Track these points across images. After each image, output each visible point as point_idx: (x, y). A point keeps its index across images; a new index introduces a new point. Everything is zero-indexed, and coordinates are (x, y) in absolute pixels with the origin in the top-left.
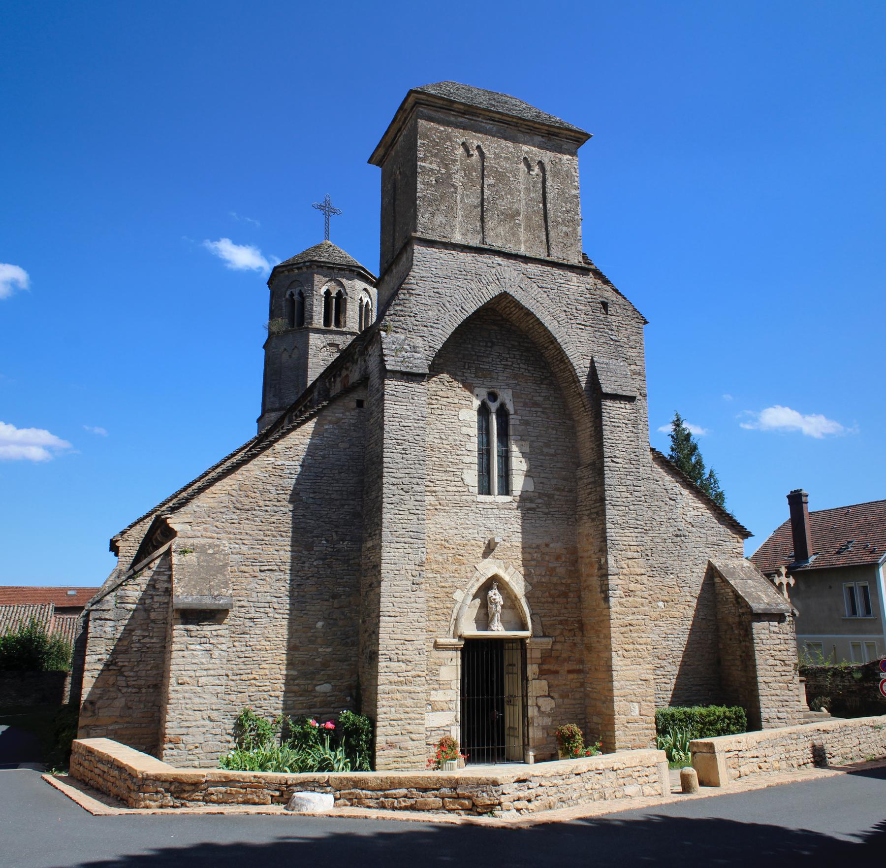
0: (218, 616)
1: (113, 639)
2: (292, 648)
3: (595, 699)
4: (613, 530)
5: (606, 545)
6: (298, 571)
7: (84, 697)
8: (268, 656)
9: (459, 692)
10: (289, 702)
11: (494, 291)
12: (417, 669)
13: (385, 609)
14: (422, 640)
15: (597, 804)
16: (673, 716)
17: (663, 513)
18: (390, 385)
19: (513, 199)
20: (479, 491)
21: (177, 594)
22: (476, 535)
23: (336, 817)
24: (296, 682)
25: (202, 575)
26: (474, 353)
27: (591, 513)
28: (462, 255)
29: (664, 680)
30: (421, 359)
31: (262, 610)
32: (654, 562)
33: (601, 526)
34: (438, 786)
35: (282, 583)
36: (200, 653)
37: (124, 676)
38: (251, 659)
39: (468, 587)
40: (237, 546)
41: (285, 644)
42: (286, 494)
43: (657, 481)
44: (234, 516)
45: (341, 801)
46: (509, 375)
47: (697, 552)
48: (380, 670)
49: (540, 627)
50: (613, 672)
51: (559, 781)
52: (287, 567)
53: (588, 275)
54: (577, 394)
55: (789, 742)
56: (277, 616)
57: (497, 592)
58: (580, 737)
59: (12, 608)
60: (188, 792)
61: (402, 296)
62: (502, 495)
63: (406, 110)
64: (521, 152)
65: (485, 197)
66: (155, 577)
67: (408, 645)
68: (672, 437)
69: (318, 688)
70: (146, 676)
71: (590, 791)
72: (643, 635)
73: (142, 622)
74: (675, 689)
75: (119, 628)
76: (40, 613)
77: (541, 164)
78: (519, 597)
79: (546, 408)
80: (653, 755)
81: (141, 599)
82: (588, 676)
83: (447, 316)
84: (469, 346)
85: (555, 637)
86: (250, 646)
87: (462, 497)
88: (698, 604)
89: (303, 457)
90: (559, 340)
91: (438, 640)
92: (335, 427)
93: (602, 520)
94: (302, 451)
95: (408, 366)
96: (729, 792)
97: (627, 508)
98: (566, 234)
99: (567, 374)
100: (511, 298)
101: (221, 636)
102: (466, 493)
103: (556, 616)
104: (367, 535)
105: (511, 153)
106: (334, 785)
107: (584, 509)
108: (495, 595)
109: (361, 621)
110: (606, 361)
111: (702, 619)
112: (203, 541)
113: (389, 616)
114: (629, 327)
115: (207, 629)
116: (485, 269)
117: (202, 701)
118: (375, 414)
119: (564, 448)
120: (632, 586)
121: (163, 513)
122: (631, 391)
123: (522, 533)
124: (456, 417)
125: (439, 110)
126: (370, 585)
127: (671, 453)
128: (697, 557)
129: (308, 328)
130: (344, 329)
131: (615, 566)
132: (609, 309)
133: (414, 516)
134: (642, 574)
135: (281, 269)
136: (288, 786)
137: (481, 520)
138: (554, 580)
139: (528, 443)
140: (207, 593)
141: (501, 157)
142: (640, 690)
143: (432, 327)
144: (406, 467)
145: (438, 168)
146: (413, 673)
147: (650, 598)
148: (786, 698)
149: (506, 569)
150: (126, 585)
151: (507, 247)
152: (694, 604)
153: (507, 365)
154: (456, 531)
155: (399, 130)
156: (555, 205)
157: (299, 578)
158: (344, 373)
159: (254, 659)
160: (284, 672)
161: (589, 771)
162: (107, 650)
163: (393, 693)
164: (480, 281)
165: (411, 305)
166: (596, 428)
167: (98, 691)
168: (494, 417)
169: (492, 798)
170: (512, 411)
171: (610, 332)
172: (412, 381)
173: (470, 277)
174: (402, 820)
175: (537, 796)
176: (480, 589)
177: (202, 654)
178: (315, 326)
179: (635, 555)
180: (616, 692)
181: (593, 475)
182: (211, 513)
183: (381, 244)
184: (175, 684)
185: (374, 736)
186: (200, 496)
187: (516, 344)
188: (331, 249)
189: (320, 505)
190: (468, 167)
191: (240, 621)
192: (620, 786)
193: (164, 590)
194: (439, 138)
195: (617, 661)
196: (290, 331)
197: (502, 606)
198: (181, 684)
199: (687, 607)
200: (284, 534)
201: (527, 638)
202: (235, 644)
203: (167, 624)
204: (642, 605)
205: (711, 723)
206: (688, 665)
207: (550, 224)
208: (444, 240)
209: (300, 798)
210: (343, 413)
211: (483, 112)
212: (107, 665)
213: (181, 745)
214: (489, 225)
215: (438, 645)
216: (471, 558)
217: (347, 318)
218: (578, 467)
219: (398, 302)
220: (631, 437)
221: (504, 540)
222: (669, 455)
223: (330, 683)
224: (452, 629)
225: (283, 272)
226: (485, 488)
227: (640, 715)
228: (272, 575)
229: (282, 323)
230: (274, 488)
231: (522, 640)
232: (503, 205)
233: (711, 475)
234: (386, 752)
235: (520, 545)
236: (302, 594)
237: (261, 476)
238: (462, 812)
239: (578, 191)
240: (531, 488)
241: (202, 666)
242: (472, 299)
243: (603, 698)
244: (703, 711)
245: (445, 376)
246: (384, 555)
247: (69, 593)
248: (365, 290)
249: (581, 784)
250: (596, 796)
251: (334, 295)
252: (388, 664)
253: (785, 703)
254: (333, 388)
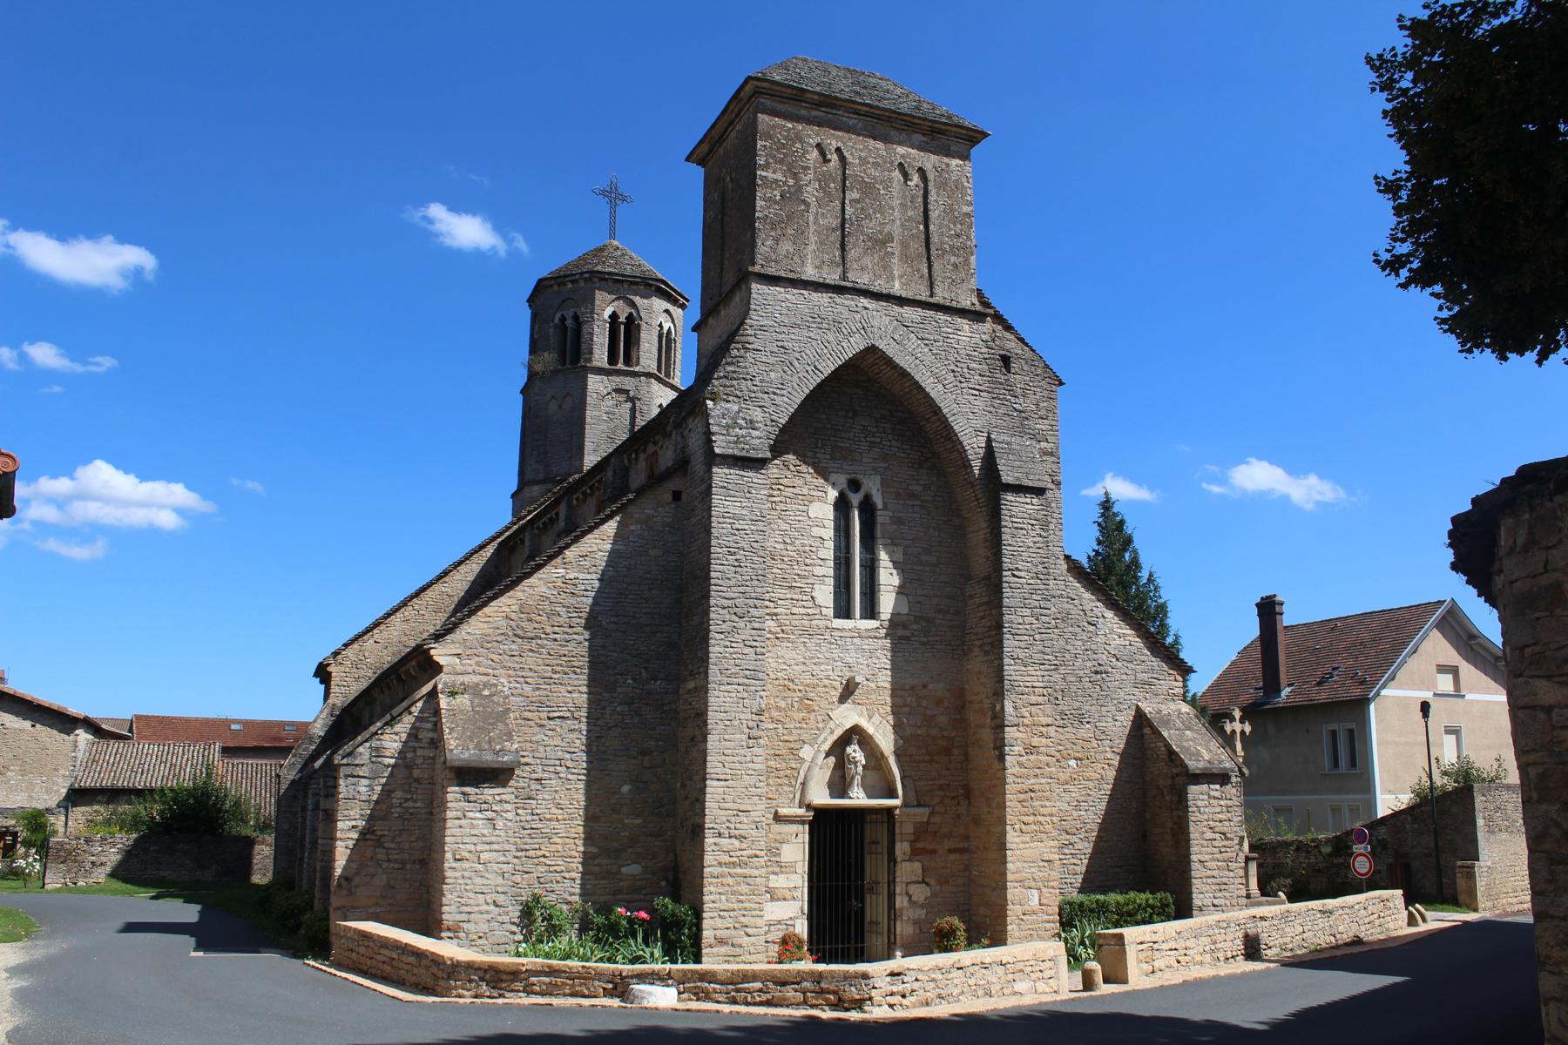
0: (501, 777)
2: (590, 819)
3: (982, 886)
4: (1012, 668)
5: (1003, 687)
6: (597, 719)
7: (338, 872)
8: (560, 827)
9: (806, 877)
10: (588, 887)
11: (857, 344)
12: (754, 847)
13: (712, 771)
14: (760, 811)
15: (981, 1001)
16: (1081, 905)
17: (1080, 643)
18: (720, 474)
19: (884, 219)
20: (834, 613)
21: (450, 747)
22: (831, 673)
23: (683, 1010)
24: (597, 861)
28: (815, 296)
29: (1073, 861)
30: (760, 438)
31: (552, 769)
34: (798, 979)
35: (576, 735)
36: (480, 822)
37: (384, 848)
38: (539, 831)
40: (518, 685)
41: (581, 813)
42: (580, 618)
43: (1073, 599)
44: (513, 647)
45: (685, 996)
47: (1122, 694)
48: (707, 848)
50: (1007, 852)
53: (984, 322)
54: (968, 483)
56: (570, 777)
57: (857, 747)
58: (963, 933)
59: (166, 747)
60: (506, 981)
61: (735, 352)
62: (866, 618)
63: (741, 100)
64: (895, 156)
65: (847, 217)
66: (418, 724)
67: (742, 816)
68: (1099, 524)
69: (624, 870)
71: (974, 987)
72: (1048, 804)
74: (1087, 871)
75: (375, 788)
76: (203, 756)
77: (921, 172)
78: (886, 755)
79: (926, 501)
80: (1050, 947)
82: (975, 856)
83: (795, 378)
84: (824, 416)
86: (537, 814)
87: (812, 622)
88: (1120, 762)
89: (602, 568)
90: (945, 411)
91: (779, 810)
92: (644, 527)
94: (601, 560)
95: (743, 449)
96: (1136, 988)
97: (1031, 638)
98: (955, 266)
99: (955, 455)
102: (817, 617)
104: (688, 673)
108: (855, 751)
109: (678, 785)
111: (1125, 781)
112: (476, 679)
114: (1038, 390)
115: (489, 793)
116: (846, 314)
117: (485, 882)
119: (950, 555)
120: (1035, 741)
121: (426, 642)
123: (892, 670)
124: (804, 514)
126: (692, 739)
128: (1121, 700)
129: (586, 366)
130: (637, 369)
131: (1014, 714)
133: (750, 649)
134: (1049, 725)
135: (547, 283)
136: (623, 978)
137: (836, 653)
138: (934, 732)
139: (900, 549)
140: (486, 747)
141: (868, 163)
142: (1041, 874)
143: (774, 393)
144: (740, 583)
145: (784, 179)
146: (749, 852)
150: (382, 734)
151: (876, 284)
152: (1116, 763)
153: (874, 442)
154: (804, 668)
155: (731, 123)
156: (940, 226)
157: (598, 728)
158: (651, 449)
159: (543, 831)
160: (581, 849)
161: (974, 964)
162: (362, 815)
164: (839, 330)
165: (747, 364)
167: (354, 866)
168: (856, 513)
169: (862, 992)
170: (880, 504)
171: (1013, 400)
173: (826, 326)
175: (913, 991)
177: (483, 824)
178: (595, 364)
179: (1040, 699)
180: (1010, 877)
181: (988, 593)
182: (484, 641)
183: (703, 272)
184: (452, 861)
186: (470, 620)
187: (888, 413)
188: (619, 253)
189: (624, 632)
191: (525, 783)
192: (1009, 982)
193: (429, 740)
194: (786, 138)
195: (1012, 837)
196: (560, 370)
197: (864, 766)
198: (459, 860)
199: (1106, 766)
200: (578, 670)
201: (896, 807)
202: (518, 811)
204: (1048, 765)
205: (1129, 914)
206: (1106, 841)
207: (933, 252)
208: (791, 275)
209: (640, 990)
210: (654, 509)
211: (845, 104)
213: (462, 935)
214: (852, 254)
215: (780, 816)
217: (641, 353)
218: (969, 580)
219: (729, 360)
221: (867, 680)
222: (1094, 550)
223: (640, 864)
224: (798, 796)
225: (551, 286)
226: (843, 610)
227: (1040, 905)
228: (563, 725)
229: (548, 358)
230: (564, 609)
231: (889, 811)
232: (870, 227)
233: (1150, 580)
234: (715, 950)
235: (888, 686)
236: (602, 749)
237: (548, 593)
238: (826, 1008)
240: (905, 610)
241: (484, 839)
242: (828, 355)
244: (1120, 898)
245: (790, 457)
246: (713, 701)
247: (233, 727)
248: (667, 311)
249: (964, 979)
250: (980, 992)
251: (622, 319)
252: (717, 840)
253: (1223, 887)
254: (633, 466)
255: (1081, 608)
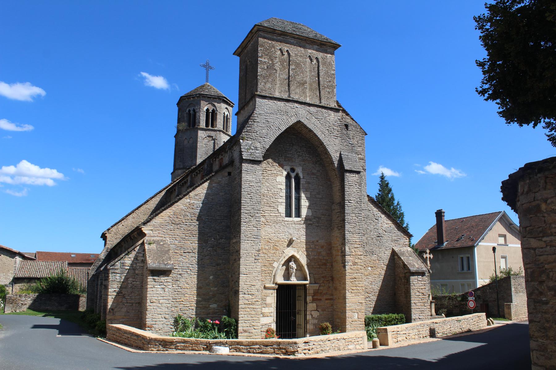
0: (167, 273)
1: (120, 282)
2: (199, 288)
3: (338, 312)
6: (201, 253)
7: (109, 307)
9: (275, 308)
10: (198, 312)
11: (293, 120)
12: (257, 298)
13: (242, 271)
14: (259, 285)
16: (373, 318)
17: (372, 226)
18: (245, 166)
23: (231, 355)
24: (201, 303)
25: (159, 254)
26: (284, 149)
27: (338, 226)
28: (279, 103)
29: (369, 303)
30: (259, 153)
31: (185, 270)
32: (367, 249)
33: (343, 233)
36: (160, 289)
37: (126, 298)
39: (280, 261)
40: (173, 241)
42: (195, 217)
43: (370, 211)
44: (171, 227)
45: (232, 350)
46: (300, 160)
48: (240, 298)
49: (313, 279)
51: (321, 343)
52: (196, 251)
53: (339, 112)
55: (420, 327)
56: (192, 273)
57: (293, 263)
58: (331, 328)
60: (168, 345)
61: (250, 123)
62: (297, 217)
63: (253, 33)
66: (137, 255)
68: (380, 184)
69: (211, 306)
70: (135, 299)
72: (361, 283)
73: (132, 275)
74: (374, 307)
77: (317, 59)
79: (318, 176)
81: (131, 265)
83: (272, 132)
84: (282, 146)
85: (320, 284)
87: (278, 219)
89: (203, 199)
91: (266, 285)
93: (343, 230)
94: (203, 196)
95: (253, 157)
98: (329, 92)
99: (328, 160)
100: (302, 123)
101: (169, 282)
102: (279, 217)
103: (321, 274)
105: (303, 53)
106: (229, 344)
107: (335, 224)
108: (292, 264)
109: (230, 276)
110: (347, 154)
111: (388, 275)
112: (158, 238)
113: (244, 274)
114: (358, 136)
115: (163, 279)
116: (290, 109)
117: (161, 310)
118: (237, 179)
120: (356, 261)
122: (358, 168)
123: (306, 235)
124: (275, 180)
125: (269, 33)
126: (235, 260)
127: (379, 193)
129: (197, 128)
130: (216, 129)
131: (349, 251)
132: (349, 128)
133: (255, 228)
134: (361, 255)
136: (210, 344)
137: (286, 229)
138: (321, 257)
140: (162, 263)
141: (298, 56)
142: (358, 307)
143: (264, 137)
144: (252, 205)
145: (268, 61)
146: (255, 300)
147: (365, 266)
148: (423, 310)
149: (298, 252)
150: (125, 258)
151: (300, 99)
152: (385, 268)
153: (300, 155)
154: (274, 235)
155: (249, 41)
157: (202, 256)
158: (220, 157)
159: (182, 292)
160: (196, 299)
163: (246, 308)
164: (287, 115)
165: (255, 127)
166: (342, 186)
167: (115, 304)
168: (293, 180)
170: (302, 177)
171: (349, 140)
172: (255, 164)
173: (283, 113)
174: (258, 357)
175: (312, 348)
176: (286, 262)
179: (358, 246)
180: (347, 308)
182: (161, 225)
185: (237, 327)
186: (156, 218)
187: (304, 144)
188: (209, 87)
189: (211, 222)
190: (282, 60)
193: (141, 260)
195: (348, 295)
196: (188, 129)
197: (296, 270)
198: (152, 302)
200: (194, 236)
201: (307, 284)
202: (173, 285)
203: (143, 276)
205: (389, 321)
206: (381, 296)
207: (321, 87)
208: (270, 96)
209: (216, 348)
210: (221, 178)
212: (118, 293)
213: (153, 329)
214: (292, 88)
216: (281, 247)
217: (217, 123)
218: (333, 204)
219: (248, 125)
220: (358, 190)
221: (297, 239)
222: (378, 193)
223: (216, 304)
224: (272, 280)
226: (289, 214)
227: (358, 318)
229: (184, 125)
230: (189, 214)
231: (305, 285)
232: (299, 78)
233: (398, 204)
235: (305, 241)
236: (203, 263)
237: (184, 208)
238: (282, 354)
239: (334, 72)
240: (310, 214)
241: (161, 295)
243: (342, 311)
244: (386, 316)
245: (270, 160)
248: (226, 108)
249: (331, 344)
250: (336, 349)
251: (211, 111)
252: (244, 295)
253: (422, 312)
255: (373, 214)
